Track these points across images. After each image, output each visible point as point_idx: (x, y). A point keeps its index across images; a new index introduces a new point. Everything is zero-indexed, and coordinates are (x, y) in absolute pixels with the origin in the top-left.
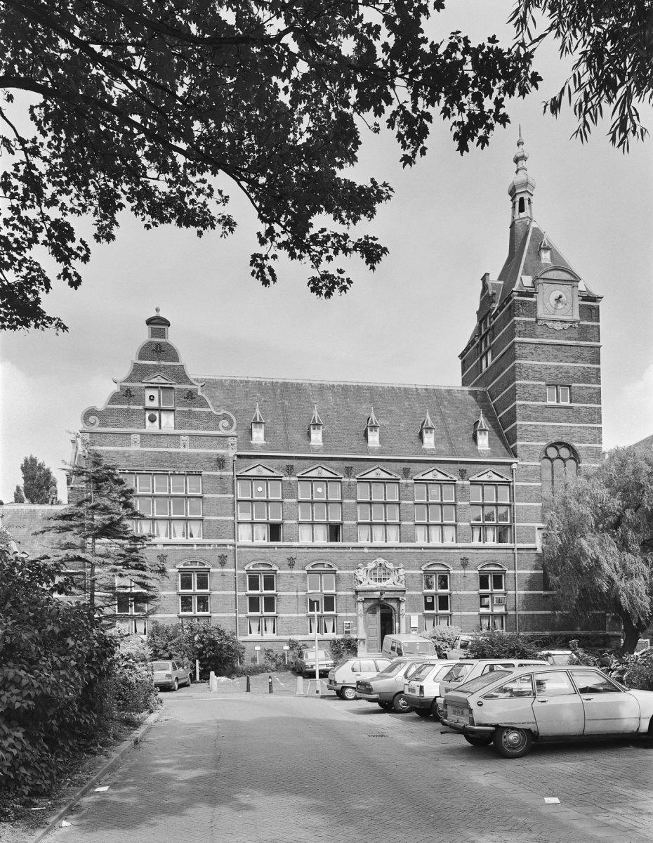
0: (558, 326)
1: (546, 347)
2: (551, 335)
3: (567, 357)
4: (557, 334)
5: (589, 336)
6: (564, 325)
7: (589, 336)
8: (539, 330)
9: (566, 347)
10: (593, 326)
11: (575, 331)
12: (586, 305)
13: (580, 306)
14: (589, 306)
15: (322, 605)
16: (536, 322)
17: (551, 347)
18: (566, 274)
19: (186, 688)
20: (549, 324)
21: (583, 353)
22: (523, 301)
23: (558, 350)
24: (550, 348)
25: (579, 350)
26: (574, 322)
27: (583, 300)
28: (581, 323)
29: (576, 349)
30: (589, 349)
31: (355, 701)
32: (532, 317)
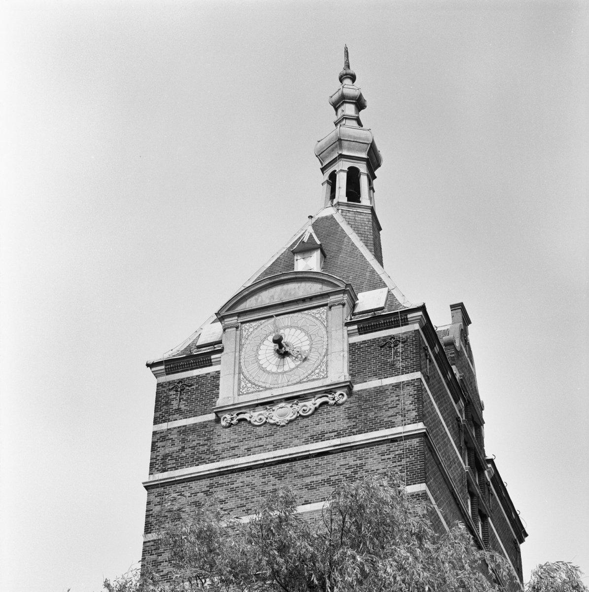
0: (282, 413)
1: (243, 478)
2: (261, 442)
3: (310, 487)
4: (279, 437)
5: (385, 415)
6: (300, 407)
7: (385, 415)
8: (225, 436)
9: (309, 462)
10: (397, 386)
11: (339, 413)
12: (374, 341)
13: (353, 348)
14: (385, 339)
15: (206, 350)
16: (218, 420)
17: (258, 473)
18: (328, 285)
19: (329, 195)
20: (255, 416)
21: (361, 466)
22: (180, 381)
23: (280, 477)
24: (256, 478)
25: (350, 459)
26: (329, 392)
27: (362, 331)
28: (357, 388)
29: (339, 461)
30: (384, 448)
31: (384, 236)
32: (204, 413)
